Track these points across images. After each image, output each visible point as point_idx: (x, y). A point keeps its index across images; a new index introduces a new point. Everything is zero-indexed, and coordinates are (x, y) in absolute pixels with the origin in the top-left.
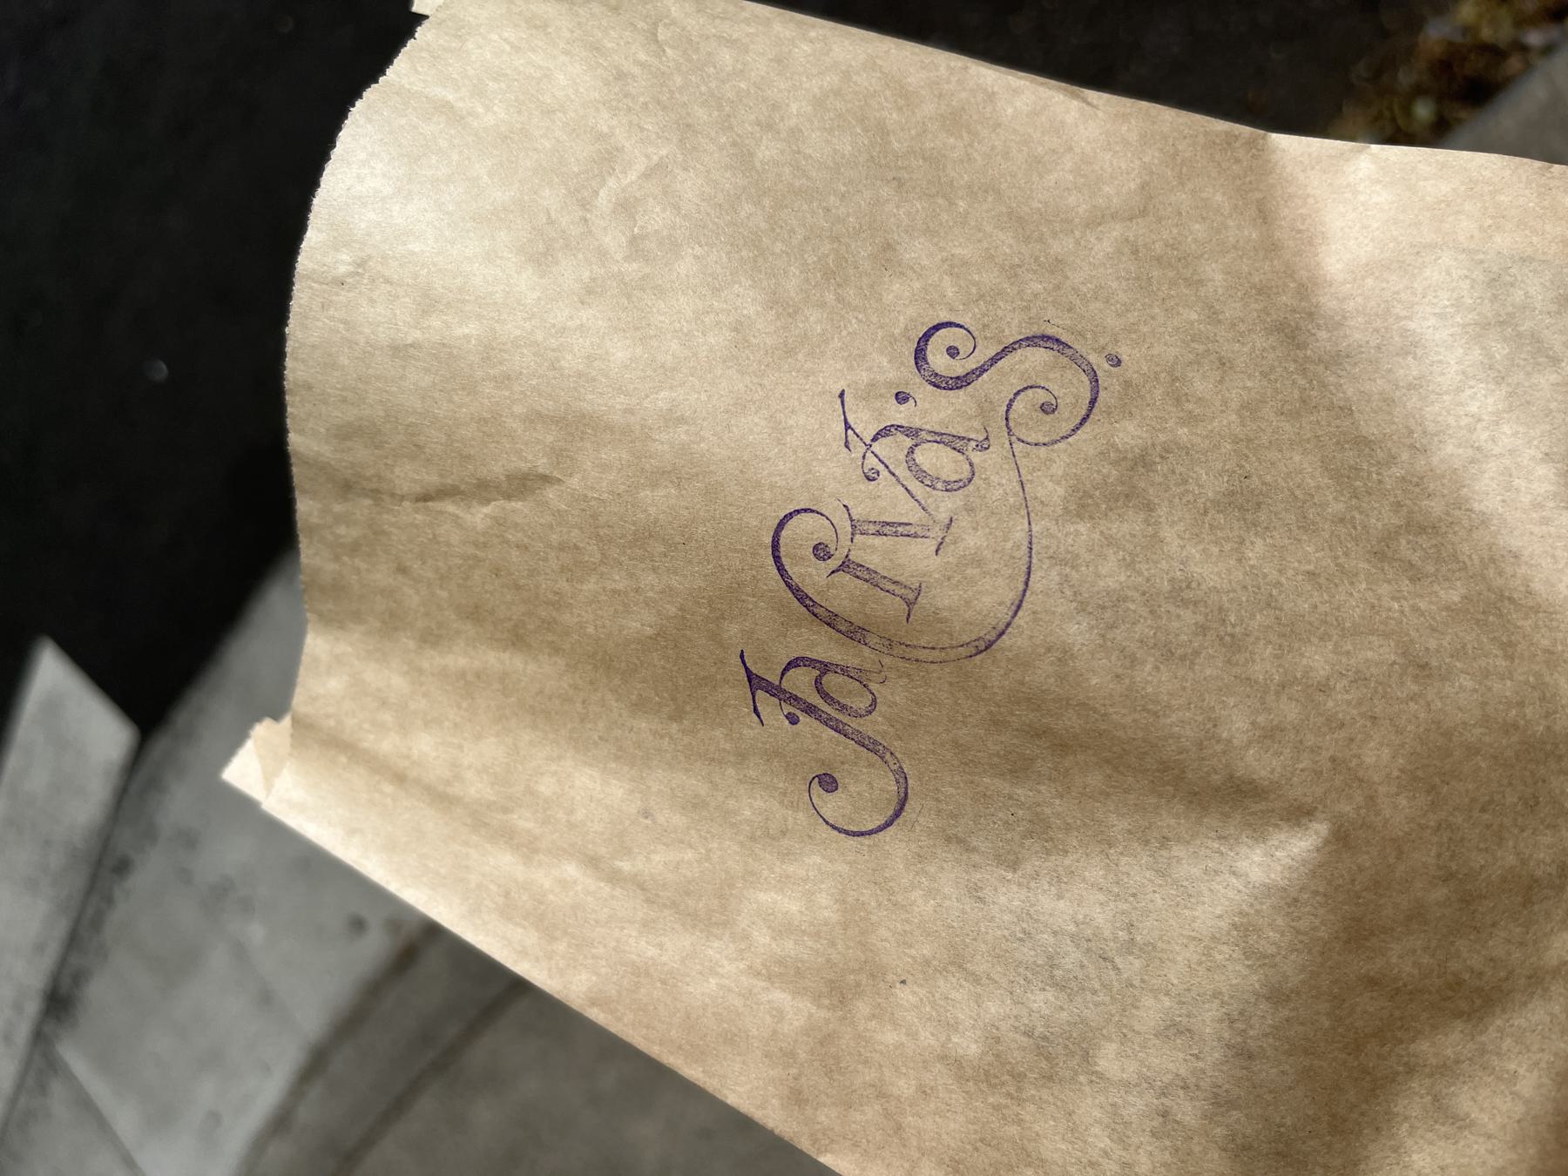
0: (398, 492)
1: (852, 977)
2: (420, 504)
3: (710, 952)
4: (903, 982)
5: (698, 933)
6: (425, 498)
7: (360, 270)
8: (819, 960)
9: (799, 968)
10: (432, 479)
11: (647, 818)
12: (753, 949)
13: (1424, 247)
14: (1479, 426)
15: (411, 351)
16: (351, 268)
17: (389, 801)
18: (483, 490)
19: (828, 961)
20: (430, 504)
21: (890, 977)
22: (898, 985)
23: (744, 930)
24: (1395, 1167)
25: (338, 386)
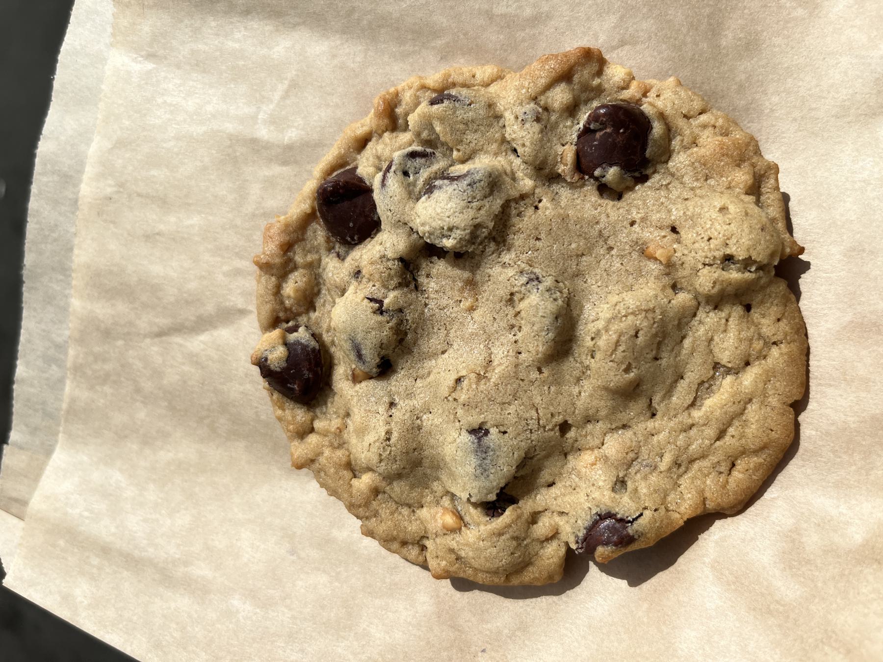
0: (142, 332)
1: (446, 653)
2: (156, 340)
3: (340, 650)
4: (484, 651)
5: (330, 637)
6: (161, 334)
7: (121, 190)
8: (421, 643)
9: (406, 653)
10: (164, 321)
11: (293, 555)
12: (371, 643)
13: (829, 54)
14: (869, 188)
15: (157, 237)
16: (115, 189)
17: (95, 571)
18: (203, 324)
19: (428, 643)
20: (164, 338)
21: (473, 649)
22: (480, 654)
23: (364, 629)
24: (630, 276)
25: (108, 264)
